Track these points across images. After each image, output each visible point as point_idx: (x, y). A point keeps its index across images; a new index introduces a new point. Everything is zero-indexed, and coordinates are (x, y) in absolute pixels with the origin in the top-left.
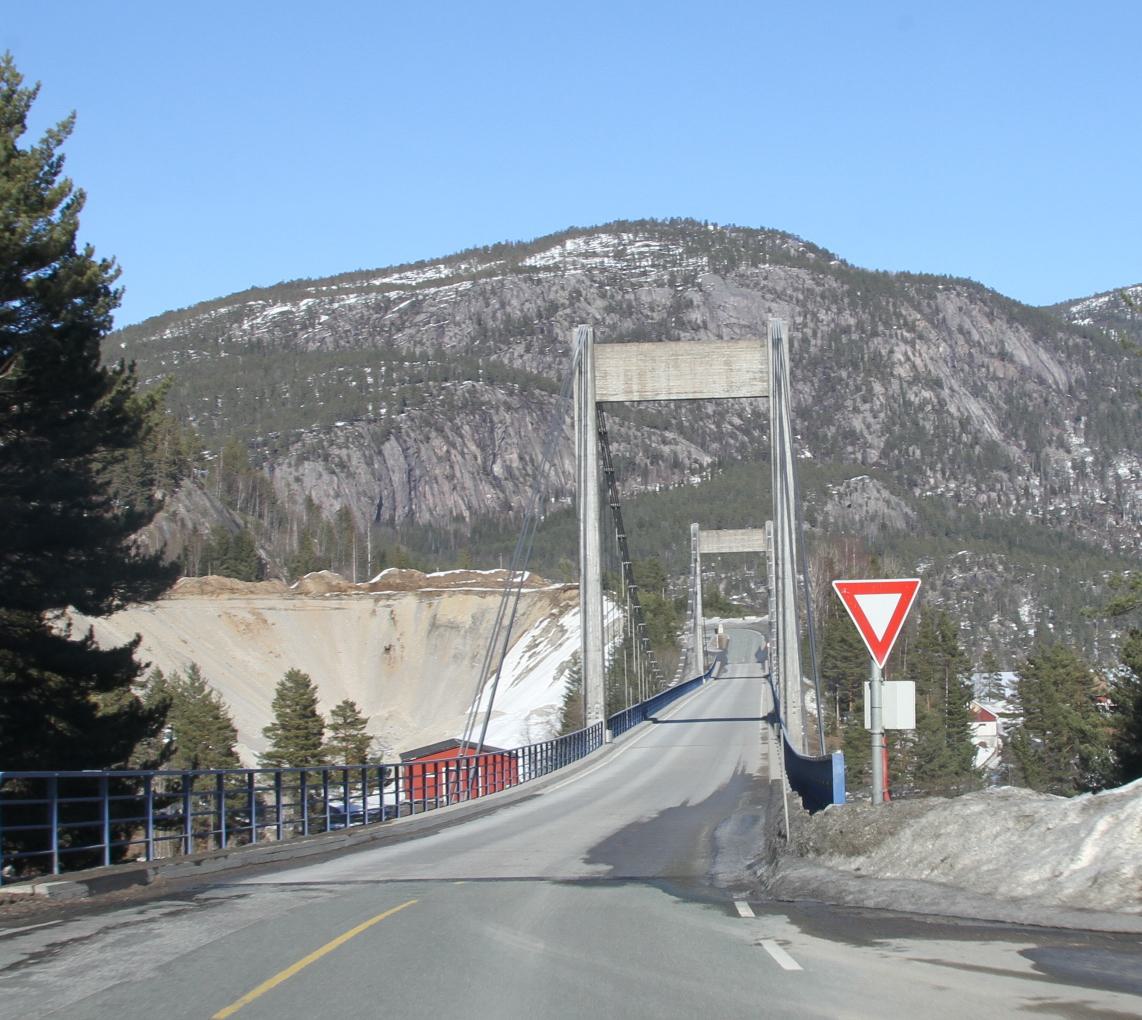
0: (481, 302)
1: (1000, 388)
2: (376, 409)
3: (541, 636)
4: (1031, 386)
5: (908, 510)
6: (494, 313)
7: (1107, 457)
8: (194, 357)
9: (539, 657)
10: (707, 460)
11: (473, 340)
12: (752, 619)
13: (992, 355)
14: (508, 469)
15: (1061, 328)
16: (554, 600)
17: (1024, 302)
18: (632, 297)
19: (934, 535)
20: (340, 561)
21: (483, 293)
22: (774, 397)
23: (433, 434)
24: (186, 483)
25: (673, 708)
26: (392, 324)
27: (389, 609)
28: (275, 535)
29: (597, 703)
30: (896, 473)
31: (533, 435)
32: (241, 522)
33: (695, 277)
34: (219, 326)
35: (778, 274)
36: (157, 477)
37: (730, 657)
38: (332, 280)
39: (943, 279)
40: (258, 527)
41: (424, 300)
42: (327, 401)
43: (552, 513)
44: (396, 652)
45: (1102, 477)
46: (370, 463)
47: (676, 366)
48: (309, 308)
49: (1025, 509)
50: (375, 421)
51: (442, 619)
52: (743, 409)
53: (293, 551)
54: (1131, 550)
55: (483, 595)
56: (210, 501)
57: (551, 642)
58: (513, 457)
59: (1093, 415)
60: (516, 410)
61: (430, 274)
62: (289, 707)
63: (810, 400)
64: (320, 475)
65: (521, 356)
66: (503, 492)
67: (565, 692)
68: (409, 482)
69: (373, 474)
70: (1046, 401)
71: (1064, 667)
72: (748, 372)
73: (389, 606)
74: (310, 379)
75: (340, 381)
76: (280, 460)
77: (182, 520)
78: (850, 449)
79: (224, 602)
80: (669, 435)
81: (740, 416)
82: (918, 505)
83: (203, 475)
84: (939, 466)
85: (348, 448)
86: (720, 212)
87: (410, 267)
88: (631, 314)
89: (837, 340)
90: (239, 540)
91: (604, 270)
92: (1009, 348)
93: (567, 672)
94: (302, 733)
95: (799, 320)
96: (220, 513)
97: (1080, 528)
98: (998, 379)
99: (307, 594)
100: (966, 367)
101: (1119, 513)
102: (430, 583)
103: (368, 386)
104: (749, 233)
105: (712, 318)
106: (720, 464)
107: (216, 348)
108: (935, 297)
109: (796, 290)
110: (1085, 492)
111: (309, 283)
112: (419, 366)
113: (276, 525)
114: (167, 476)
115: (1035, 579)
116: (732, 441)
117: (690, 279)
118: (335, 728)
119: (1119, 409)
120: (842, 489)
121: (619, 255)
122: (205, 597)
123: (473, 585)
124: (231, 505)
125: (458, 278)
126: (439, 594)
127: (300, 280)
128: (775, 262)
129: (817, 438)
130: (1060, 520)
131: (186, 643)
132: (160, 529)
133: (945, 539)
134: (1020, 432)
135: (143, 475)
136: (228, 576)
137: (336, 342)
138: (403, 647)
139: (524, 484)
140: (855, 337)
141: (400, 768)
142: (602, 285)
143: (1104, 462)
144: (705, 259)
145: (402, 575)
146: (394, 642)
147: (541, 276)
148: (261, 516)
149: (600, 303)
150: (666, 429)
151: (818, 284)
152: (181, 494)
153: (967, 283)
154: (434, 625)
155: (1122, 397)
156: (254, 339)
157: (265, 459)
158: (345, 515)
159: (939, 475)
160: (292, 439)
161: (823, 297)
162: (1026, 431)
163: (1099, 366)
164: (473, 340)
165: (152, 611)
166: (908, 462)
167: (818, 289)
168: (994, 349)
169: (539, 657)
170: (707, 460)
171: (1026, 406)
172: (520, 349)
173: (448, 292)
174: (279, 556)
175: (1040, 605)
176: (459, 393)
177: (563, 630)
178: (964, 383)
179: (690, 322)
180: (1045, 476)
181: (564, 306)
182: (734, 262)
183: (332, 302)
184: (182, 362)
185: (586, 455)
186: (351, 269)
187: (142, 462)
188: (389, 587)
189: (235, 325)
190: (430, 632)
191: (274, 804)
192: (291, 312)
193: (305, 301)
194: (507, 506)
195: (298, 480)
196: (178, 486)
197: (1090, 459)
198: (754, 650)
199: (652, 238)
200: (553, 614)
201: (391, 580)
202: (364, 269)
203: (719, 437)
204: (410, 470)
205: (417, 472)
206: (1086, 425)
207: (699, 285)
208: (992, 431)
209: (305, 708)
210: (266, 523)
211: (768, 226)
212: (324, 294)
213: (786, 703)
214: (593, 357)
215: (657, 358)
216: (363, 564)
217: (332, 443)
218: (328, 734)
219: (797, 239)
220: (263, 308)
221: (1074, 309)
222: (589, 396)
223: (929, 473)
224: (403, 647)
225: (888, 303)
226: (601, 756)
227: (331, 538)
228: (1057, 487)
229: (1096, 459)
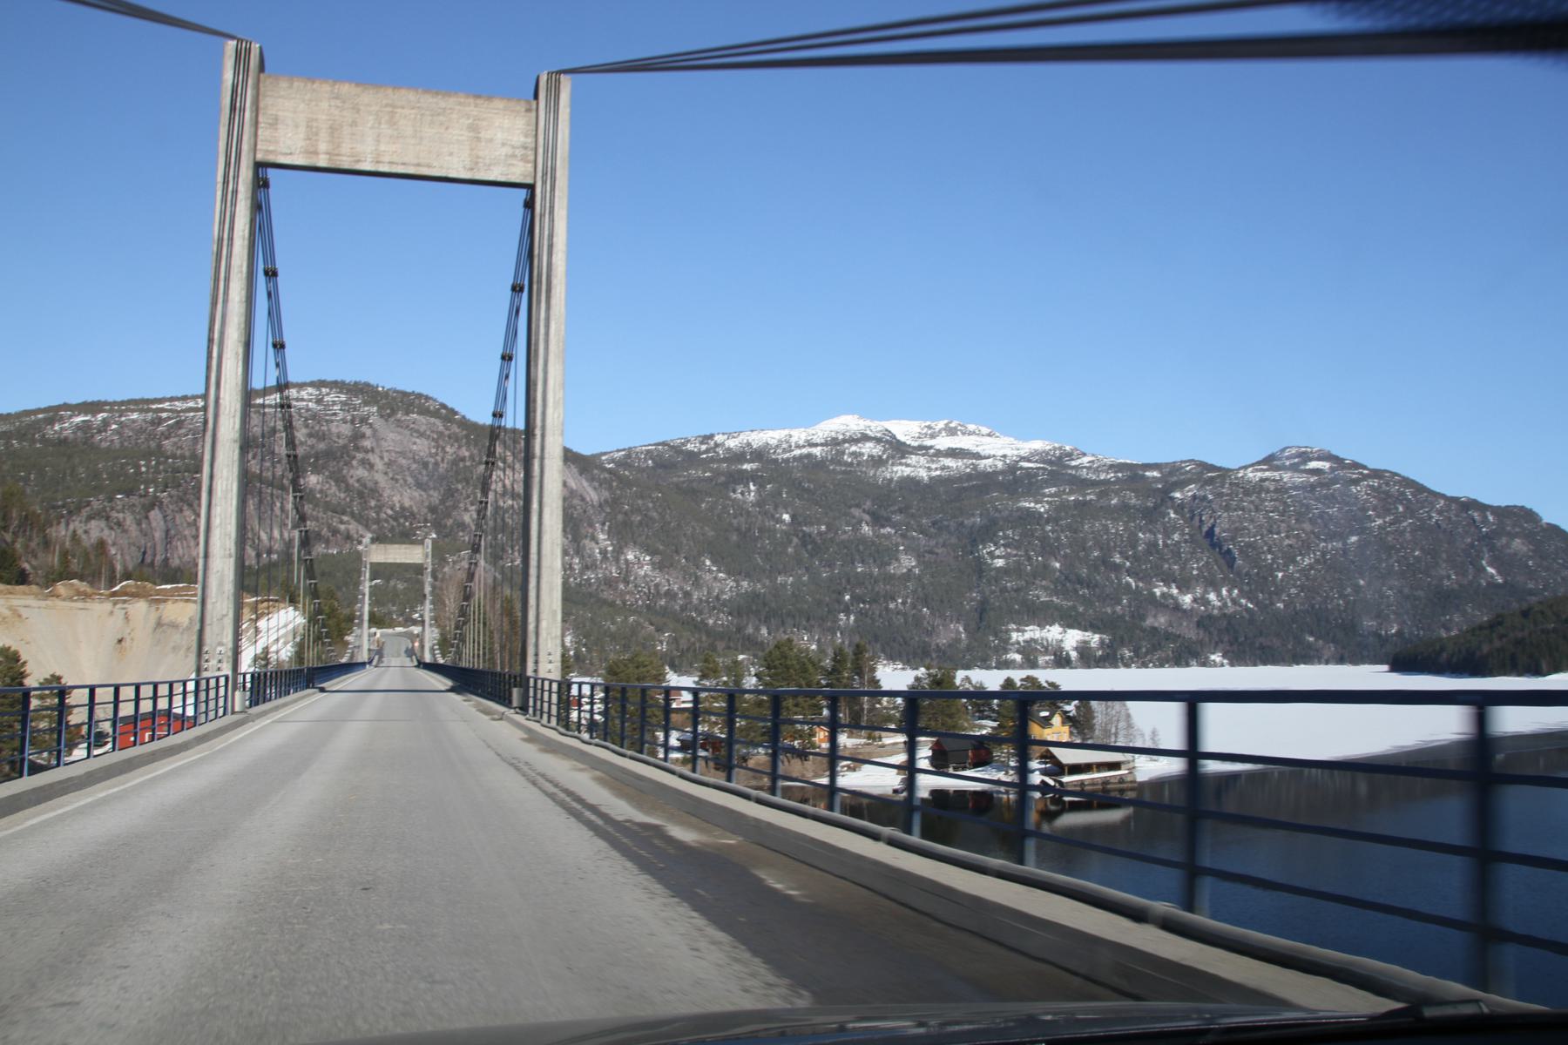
2: (147, 488)
7: (621, 548)
17: (575, 450)
23: (185, 508)
27: (124, 611)
29: (220, 644)
33: (368, 419)
34: (36, 426)
37: (385, 652)
38: (122, 403)
40: (26, 547)
41: (185, 420)
44: (126, 644)
45: (617, 560)
46: (139, 523)
47: (392, 123)
48: (104, 420)
50: (145, 496)
51: (165, 620)
61: (191, 404)
63: (437, 502)
68: (166, 538)
69: (141, 531)
70: (585, 512)
72: (503, 144)
73: (124, 609)
74: (100, 466)
75: (122, 469)
76: (74, 518)
78: (461, 534)
80: (345, 518)
81: (392, 509)
85: (123, 512)
86: (387, 379)
87: (178, 399)
89: (457, 465)
91: (308, 410)
95: (434, 451)
97: (602, 591)
101: (627, 582)
102: (159, 592)
103: (142, 473)
104: (405, 394)
107: (34, 441)
109: (433, 432)
111: (106, 403)
112: (179, 463)
115: (575, 620)
117: (364, 420)
120: (455, 558)
121: (319, 401)
126: (165, 601)
127: (99, 401)
128: (420, 413)
130: (590, 584)
137: (122, 443)
138: (132, 639)
140: (468, 464)
142: (306, 419)
143: (619, 551)
144: (375, 408)
145: (137, 587)
146: (126, 636)
149: (304, 431)
154: (159, 624)
155: (632, 511)
156: (62, 437)
161: (449, 437)
163: (618, 492)
167: (447, 433)
171: (572, 514)
175: (577, 636)
180: (582, 558)
182: (394, 412)
183: (120, 416)
185: (231, 239)
186: (137, 396)
188: (126, 594)
190: (155, 629)
195: (86, 532)
197: (610, 548)
198: (404, 649)
199: (341, 392)
201: (128, 590)
205: (173, 532)
206: (609, 527)
207: (371, 424)
211: (417, 390)
212: (117, 411)
213: (537, 655)
215: (362, 108)
217: (112, 509)
219: (435, 400)
220: (71, 417)
221: (604, 458)
222: (245, 147)
224: (132, 639)
227: (87, 560)
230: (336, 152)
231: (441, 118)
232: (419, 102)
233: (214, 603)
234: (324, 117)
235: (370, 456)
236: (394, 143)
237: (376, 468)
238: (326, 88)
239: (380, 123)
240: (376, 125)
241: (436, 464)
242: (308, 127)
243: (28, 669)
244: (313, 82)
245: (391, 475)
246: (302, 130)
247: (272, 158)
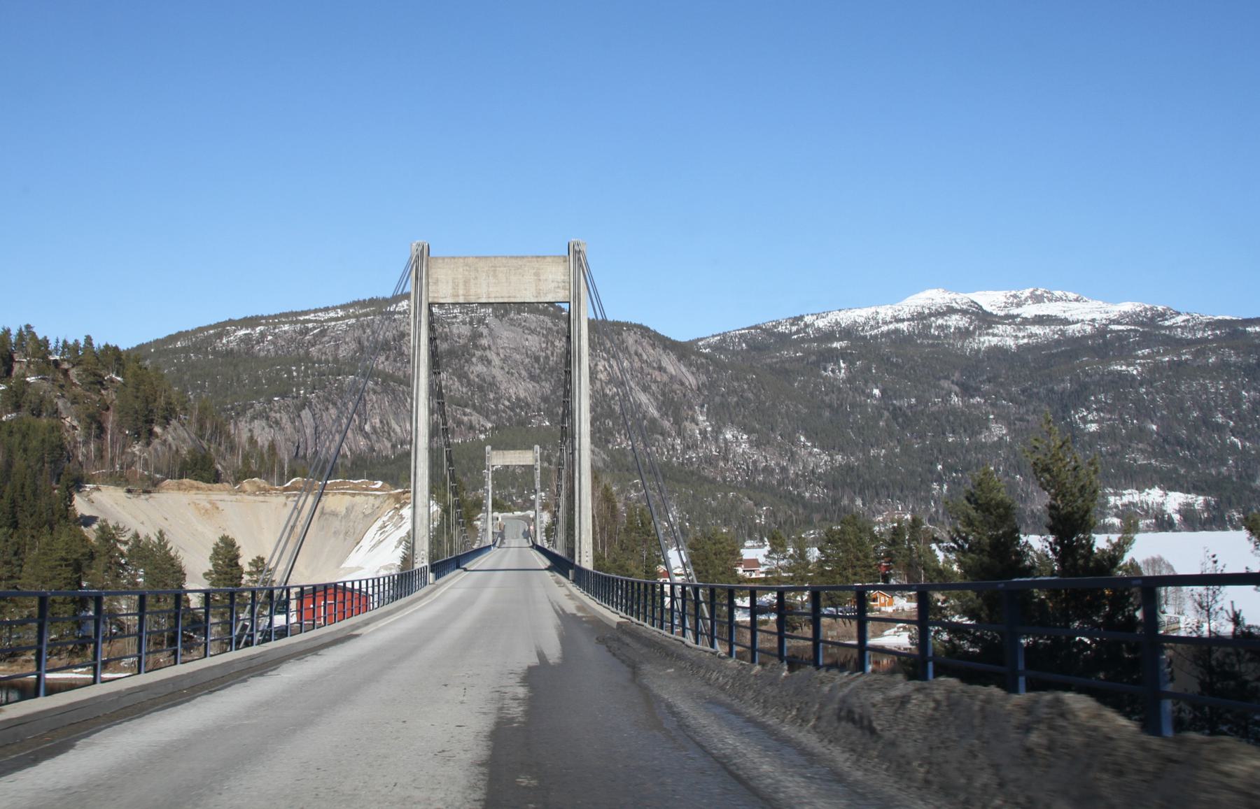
0: (361, 331)
1: (658, 387)
2: (298, 391)
3: (388, 521)
4: (676, 386)
5: (605, 456)
6: (368, 337)
7: (719, 428)
8: (193, 358)
9: (387, 534)
10: (489, 425)
11: (356, 352)
12: (518, 513)
13: (654, 368)
14: (374, 428)
15: (694, 353)
16: (397, 498)
17: (673, 338)
18: (448, 330)
19: (620, 470)
20: (267, 474)
21: (362, 326)
22: (574, 302)
23: (331, 406)
24: (174, 422)
25: (477, 562)
26: (309, 342)
28: (228, 457)
29: (423, 550)
30: (598, 435)
31: (388, 408)
32: (206, 447)
33: (485, 319)
34: (208, 341)
36: (156, 418)
38: (275, 316)
39: (626, 324)
40: (217, 451)
42: (269, 386)
43: (398, 455)
45: (716, 440)
46: (293, 422)
47: (495, 276)
48: (261, 332)
49: (672, 457)
52: (511, 397)
53: (238, 466)
54: (733, 481)
55: (353, 495)
56: (188, 434)
57: (395, 525)
58: (377, 421)
59: (711, 404)
60: (379, 394)
61: (332, 314)
62: (221, 559)
63: (549, 392)
64: (264, 428)
65: (383, 363)
66: (370, 441)
67: (401, 555)
69: (295, 429)
70: (684, 395)
71: (721, 543)
75: (277, 374)
76: (241, 419)
77: (170, 445)
79: (192, 496)
80: (468, 410)
81: (509, 401)
82: (611, 454)
83: (185, 419)
84: (623, 431)
85: (280, 412)
87: (321, 310)
88: (447, 340)
90: (204, 457)
92: (664, 364)
93: (404, 543)
94: (228, 577)
96: (193, 441)
97: (703, 469)
98: (658, 382)
99: (244, 492)
100: (639, 375)
101: (726, 460)
105: (494, 344)
106: (497, 428)
107: (207, 353)
108: (622, 334)
109: (542, 328)
110: (707, 448)
111: (262, 317)
113: (229, 450)
114: (162, 417)
115: (678, 497)
116: (504, 415)
117: (481, 321)
118: (250, 574)
119: (726, 400)
122: (181, 492)
123: (347, 489)
124: (202, 437)
125: (348, 317)
127: (257, 316)
128: (530, 312)
129: (553, 414)
130: (692, 463)
131: (166, 519)
132: (156, 450)
133: (626, 473)
134: (670, 413)
135: (146, 416)
136: (196, 480)
137: (276, 352)
139: (383, 437)
141: (701, 591)
143: (718, 431)
144: (491, 310)
147: (396, 316)
148: (220, 445)
150: (466, 407)
151: (555, 325)
152: (170, 429)
153: (640, 327)
155: (728, 393)
156: (229, 349)
157: (232, 418)
158: (272, 447)
159: (623, 437)
160: (248, 407)
161: (558, 332)
162: (673, 412)
164: (356, 352)
165: (147, 500)
166: (605, 429)
167: (555, 328)
168: (655, 365)
169: (387, 534)
170: (489, 425)
171: (673, 398)
172: (382, 358)
173: (342, 325)
174: (230, 469)
175: (681, 512)
176: (347, 382)
177: (402, 518)
178: (638, 384)
179: (481, 345)
180: (684, 438)
182: (507, 312)
183: (274, 329)
184: (186, 361)
185: (419, 346)
187: (147, 409)
188: (296, 489)
189: (218, 341)
191: (36, 643)
192: (251, 334)
193: (259, 328)
194: (372, 449)
196: (169, 424)
200: (396, 508)
202: (294, 310)
203: (496, 412)
204: (316, 427)
207: (487, 325)
208: (653, 412)
209: (231, 560)
210: (222, 448)
212: (271, 324)
214: (427, 265)
216: (282, 475)
217: (271, 410)
218: (246, 577)
220: (235, 331)
221: (700, 343)
222: (423, 298)
223: (617, 435)
225: (594, 337)
226: (426, 595)
228: (690, 445)
229: (713, 429)
235: (488, 353)
237: (493, 363)
243: (241, 552)
245: (507, 370)
246: (450, 284)
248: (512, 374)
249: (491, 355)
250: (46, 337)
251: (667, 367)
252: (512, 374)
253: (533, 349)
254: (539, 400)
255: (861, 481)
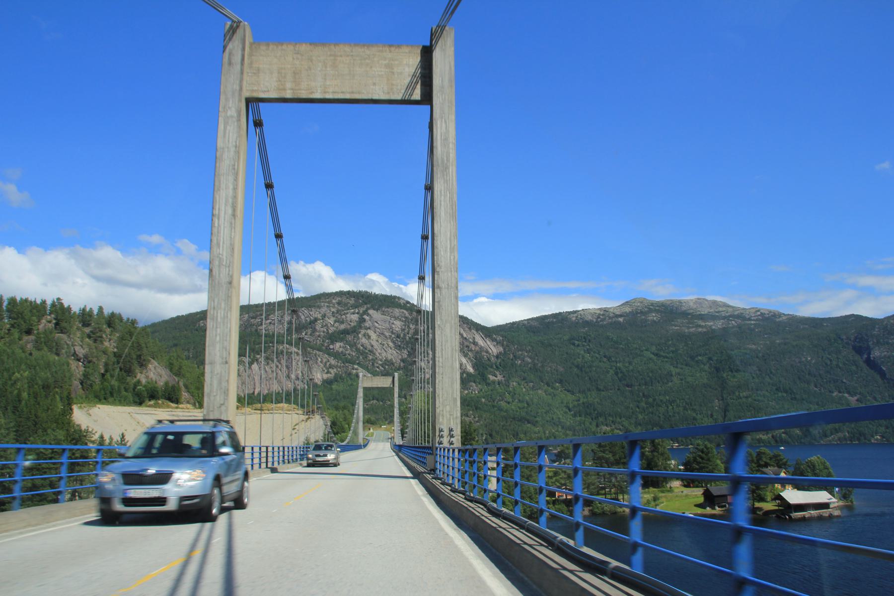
35: (397, 312)
63: (406, 356)
92: (476, 340)
98: (472, 350)
116: (378, 369)
168: (471, 340)
181: (320, 320)
230: (297, 88)
231: (367, 61)
232: (352, 52)
233: (214, 396)
234: (289, 66)
235: (369, 331)
236: (336, 79)
237: (372, 338)
238: (291, 47)
239: (326, 67)
240: (324, 69)
241: (405, 335)
242: (279, 73)
244: (282, 44)
245: (380, 342)
247: (255, 95)
248: (383, 345)
249: (370, 332)
250: (69, 306)
251: (479, 342)
252: (383, 345)
253: (397, 329)
254: (399, 361)
255: (596, 412)
